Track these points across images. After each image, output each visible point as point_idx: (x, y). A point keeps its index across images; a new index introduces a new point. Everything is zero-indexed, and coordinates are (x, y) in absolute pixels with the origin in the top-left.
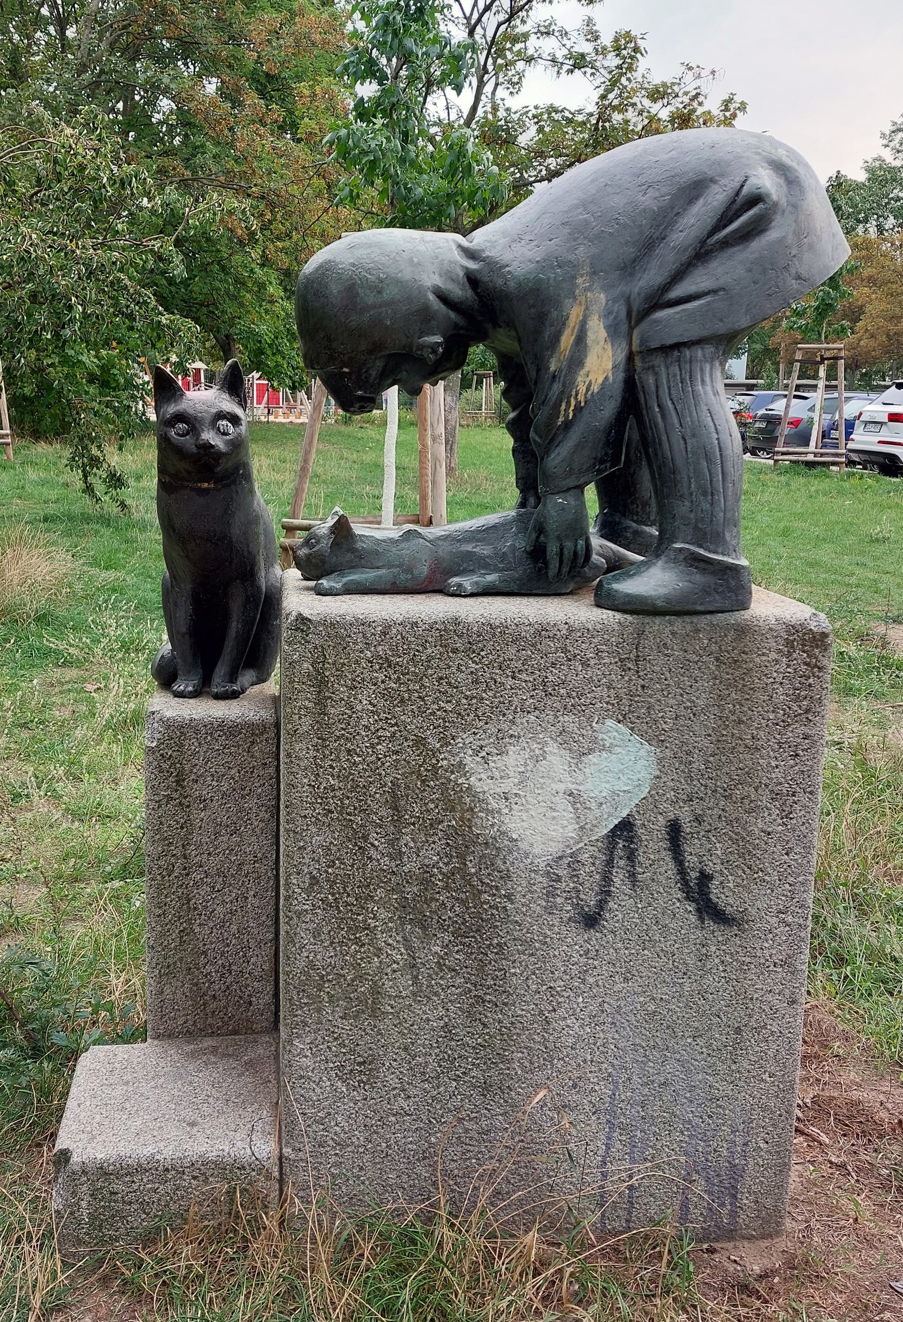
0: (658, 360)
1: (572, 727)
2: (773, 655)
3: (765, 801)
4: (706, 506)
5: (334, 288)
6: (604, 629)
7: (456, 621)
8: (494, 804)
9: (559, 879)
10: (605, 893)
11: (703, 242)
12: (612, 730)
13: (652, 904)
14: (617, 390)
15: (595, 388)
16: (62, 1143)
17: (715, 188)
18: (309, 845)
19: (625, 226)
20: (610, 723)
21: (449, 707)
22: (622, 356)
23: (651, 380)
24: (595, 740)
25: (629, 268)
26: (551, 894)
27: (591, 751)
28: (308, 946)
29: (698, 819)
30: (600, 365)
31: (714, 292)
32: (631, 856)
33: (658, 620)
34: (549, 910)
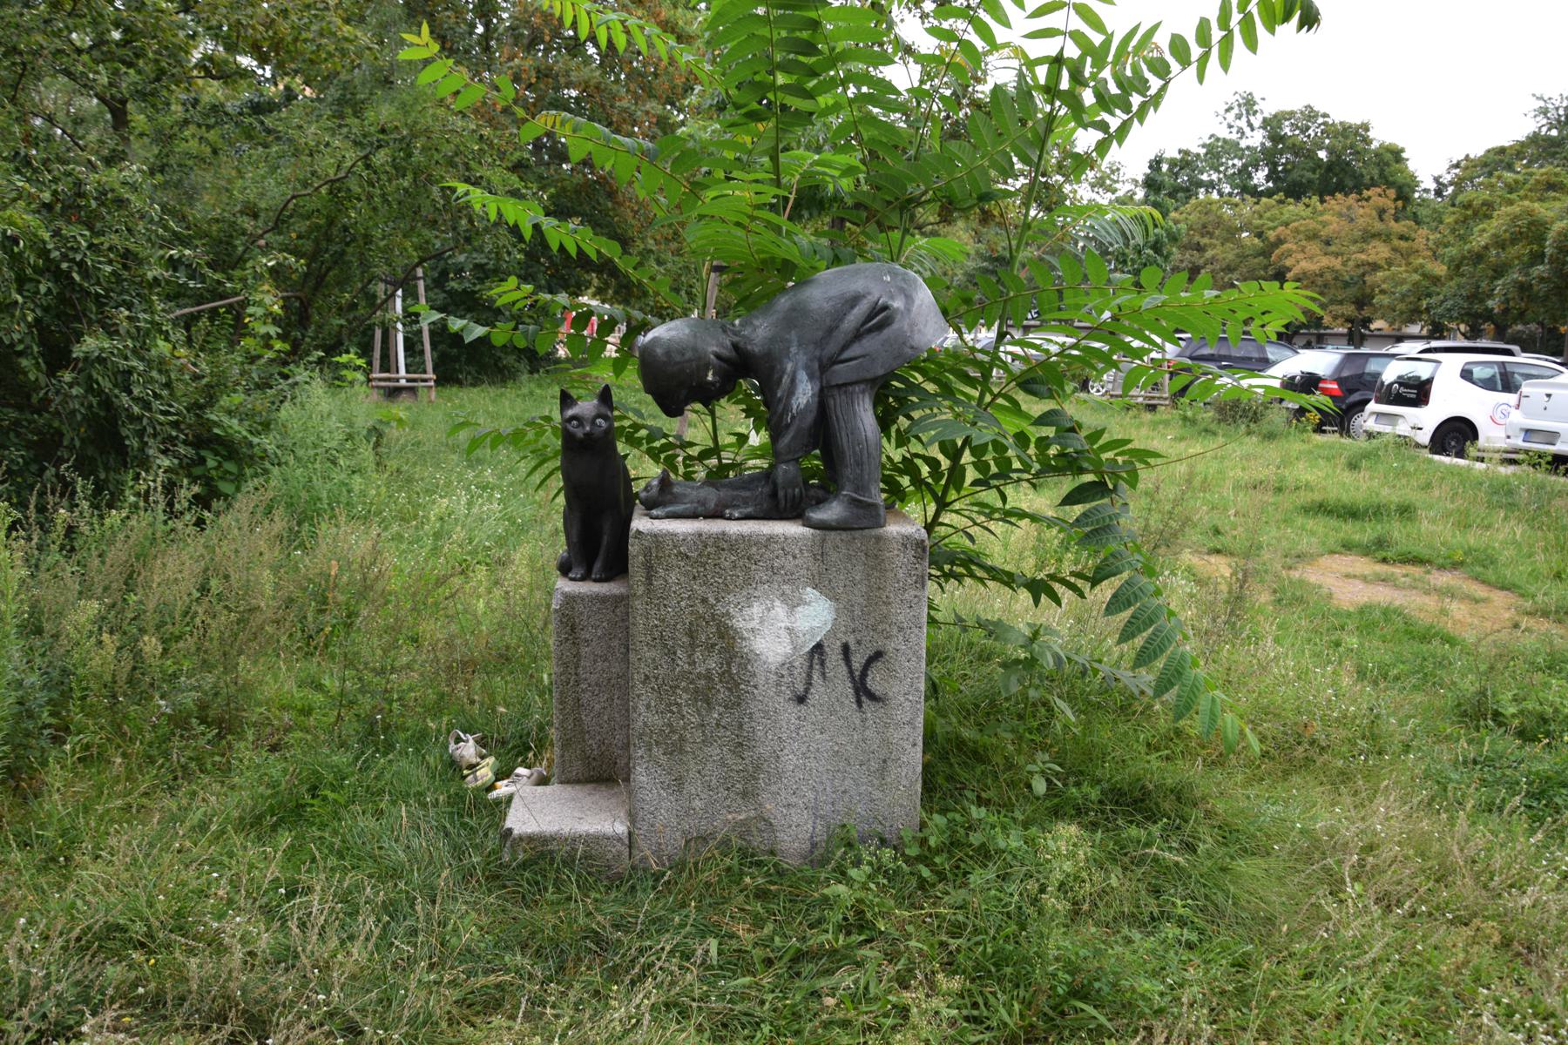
0: (835, 392)
5: (659, 351)
6: (804, 537)
7: (724, 534)
10: (809, 684)
11: (858, 330)
12: (810, 593)
13: (835, 688)
14: (814, 407)
16: (508, 824)
18: (646, 656)
22: (817, 389)
25: (820, 344)
26: (778, 685)
28: (646, 714)
29: (859, 643)
30: (804, 394)
32: (822, 663)
34: (778, 693)
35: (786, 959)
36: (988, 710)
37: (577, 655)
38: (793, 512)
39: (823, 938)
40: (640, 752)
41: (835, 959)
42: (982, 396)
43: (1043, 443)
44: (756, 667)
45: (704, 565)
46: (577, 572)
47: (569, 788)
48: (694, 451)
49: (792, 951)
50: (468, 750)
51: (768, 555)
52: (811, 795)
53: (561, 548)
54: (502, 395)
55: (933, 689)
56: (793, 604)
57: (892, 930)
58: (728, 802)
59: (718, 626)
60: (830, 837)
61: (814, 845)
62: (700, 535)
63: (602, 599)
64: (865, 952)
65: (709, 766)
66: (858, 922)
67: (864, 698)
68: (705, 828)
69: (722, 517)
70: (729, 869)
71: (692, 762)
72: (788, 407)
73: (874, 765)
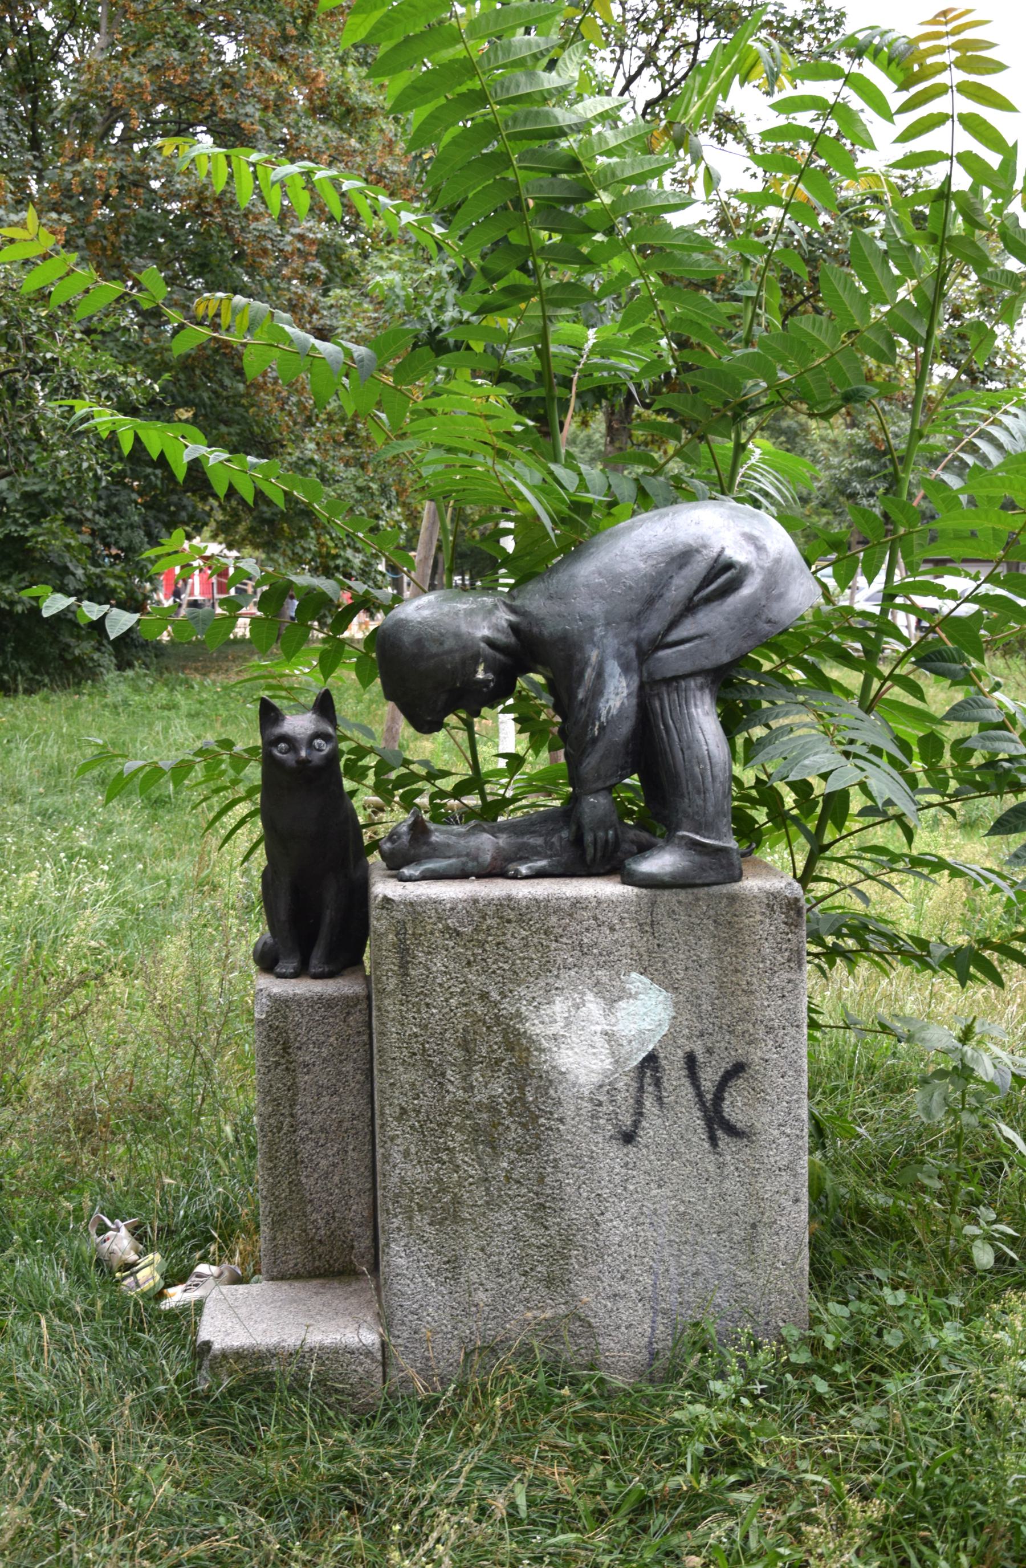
1: (605, 980)
2: (759, 917)
3: (761, 1033)
4: (700, 802)
5: (407, 639)
6: (626, 901)
7: (509, 898)
8: (545, 1044)
9: (600, 1104)
10: (639, 1114)
11: (691, 599)
12: (636, 981)
13: (675, 1120)
15: (614, 711)
16: (204, 1335)
17: (699, 557)
18: (399, 1081)
19: (631, 588)
20: (634, 975)
21: (506, 967)
23: (657, 704)
24: (623, 990)
25: (636, 619)
27: (620, 998)
28: (403, 1165)
29: (709, 1051)
30: (617, 694)
31: (700, 636)
32: (657, 1083)
33: (667, 892)
34: (594, 1130)
35: (625, 1509)
36: (897, 1166)
37: (293, 1087)
38: (609, 863)
39: (680, 1479)
40: (396, 1222)
41: (696, 1507)
42: (866, 685)
43: (962, 750)
44: (561, 1091)
45: (482, 944)
46: (288, 966)
47: (285, 1286)
48: (447, 784)
49: (633, 1498)
50: (120, 1242)
51: (574, 927)
52: (647, 1280)
53: (257, 932)
54: (77, 706)
55: (819, 1131)
56: (612, 997)
57: (778, 1468)
58: (525, 1294)
59: (505, 1033)
60: (676, 1342)
61: (654, 1355)
62: (475, 901)
63: (328, 1003)
64: (742, 1496)
65: (497, 1240)
66: (727, 1457)
67: (720, 1133)
68: (493, 1330)
69: (503, 875)
70: (531, 1391)
71: (472, 1237)
72: (593, 715)
73: (738, 1233)
